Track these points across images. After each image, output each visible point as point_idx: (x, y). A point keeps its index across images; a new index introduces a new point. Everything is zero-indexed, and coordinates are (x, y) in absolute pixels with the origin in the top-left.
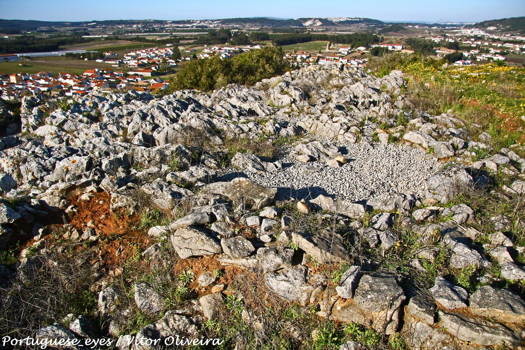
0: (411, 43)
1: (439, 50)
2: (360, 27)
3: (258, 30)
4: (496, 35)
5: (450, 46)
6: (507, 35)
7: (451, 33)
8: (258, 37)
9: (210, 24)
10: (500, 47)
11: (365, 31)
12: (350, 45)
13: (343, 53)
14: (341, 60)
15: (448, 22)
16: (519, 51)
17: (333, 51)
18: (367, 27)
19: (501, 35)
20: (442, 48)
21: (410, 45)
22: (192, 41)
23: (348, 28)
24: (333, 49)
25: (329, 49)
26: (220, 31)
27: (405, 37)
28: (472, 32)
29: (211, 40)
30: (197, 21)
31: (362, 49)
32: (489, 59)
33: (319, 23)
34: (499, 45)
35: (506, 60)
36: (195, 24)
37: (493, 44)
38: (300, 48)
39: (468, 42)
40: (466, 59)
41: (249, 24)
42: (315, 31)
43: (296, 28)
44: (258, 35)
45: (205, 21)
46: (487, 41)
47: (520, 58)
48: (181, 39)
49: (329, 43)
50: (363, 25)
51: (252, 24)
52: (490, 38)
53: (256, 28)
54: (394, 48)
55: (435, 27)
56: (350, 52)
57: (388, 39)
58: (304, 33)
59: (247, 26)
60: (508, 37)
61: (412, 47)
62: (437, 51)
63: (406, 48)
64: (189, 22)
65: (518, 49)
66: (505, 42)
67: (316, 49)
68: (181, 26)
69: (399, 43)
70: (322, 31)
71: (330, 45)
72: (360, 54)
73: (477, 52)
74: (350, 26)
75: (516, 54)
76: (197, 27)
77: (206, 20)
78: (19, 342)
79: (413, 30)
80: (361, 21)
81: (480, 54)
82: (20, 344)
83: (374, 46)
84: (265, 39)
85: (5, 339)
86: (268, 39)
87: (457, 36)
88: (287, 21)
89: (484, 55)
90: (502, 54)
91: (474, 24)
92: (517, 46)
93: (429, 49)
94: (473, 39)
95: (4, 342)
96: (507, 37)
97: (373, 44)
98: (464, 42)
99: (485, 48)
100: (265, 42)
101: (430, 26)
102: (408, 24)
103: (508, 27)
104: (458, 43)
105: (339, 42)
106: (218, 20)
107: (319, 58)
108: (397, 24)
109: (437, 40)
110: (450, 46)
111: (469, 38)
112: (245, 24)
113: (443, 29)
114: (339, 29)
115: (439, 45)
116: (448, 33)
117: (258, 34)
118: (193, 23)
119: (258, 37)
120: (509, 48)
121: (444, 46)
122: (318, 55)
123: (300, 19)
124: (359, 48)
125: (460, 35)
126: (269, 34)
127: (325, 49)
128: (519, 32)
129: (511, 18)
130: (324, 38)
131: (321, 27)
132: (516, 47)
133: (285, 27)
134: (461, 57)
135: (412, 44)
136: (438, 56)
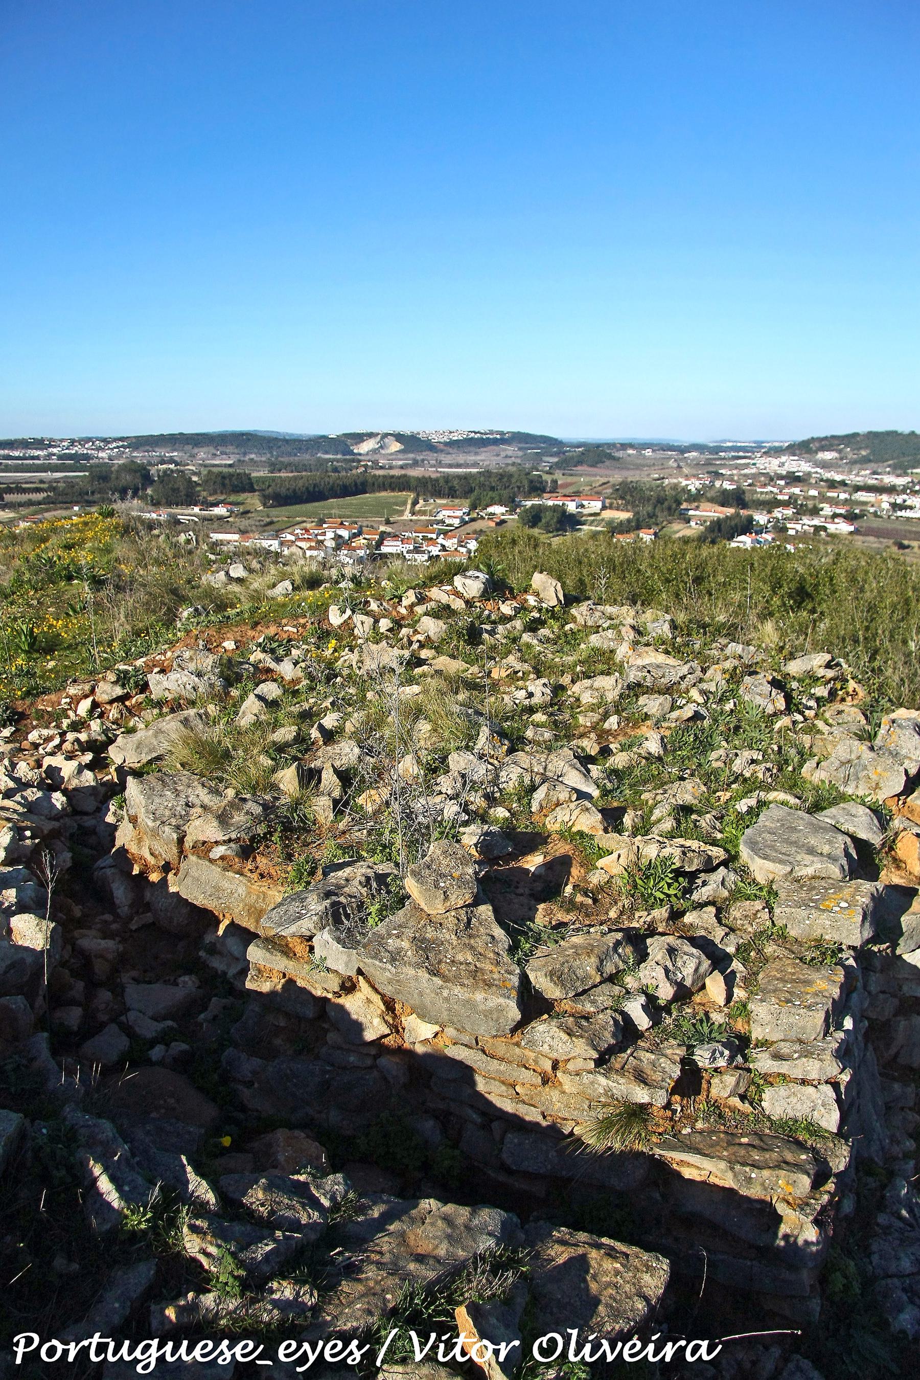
0: (626, 494)
1: (697, 508)
2: (503, 454)
3: (230, 466)
4: (838, 473)
5: (724, 499)
6: (863, 473)
7: (732, 467)
8: (224, 485)
9: (99, 449)
10: (846, 500)
11: (513, 464)
12: (467, 503)
13: (448, 521)
14: (441, 540)
15: (725, 441)
16: (888, 510)
17: (423, 518)
18: (520, 453)
19: (850, 472)
20: (705, 505)
21: (622, 498)
22: (40, 496)
23: (471, 458)
24: (423, 513)
25: (413, 514)
26: (123, 468)
27: (617, 477)
28: (782, 465)
29: (93, 493)
30: (62, 440)
31: (498, 510)
32: (817, 529)
33: (396, 446)
34: (843, 496)
35: (857, 532)
36: (55, 450)
37: (829, 494)
38: (333, 511)
39: (769, 488)
40: (761, 530)
41: (205, 449)
42: (381, 468)
43: (332, 461)
44: (224, 478)
45: (83, 441)
46: (815, 486)
47: (889, 526)
48: (10, 490)
49: (412, 496)
50: (510, 450)
51: (216, 448)
52: (822, 480)
53: (224, 461)
54: (583, 506)
55: (694, 454)
56: (467, 518)
57: (571, 484)
58: (354, 472)
59: (201, 453)
60: (865, 476)
61: (628, 503)
62: (691, 513)
63: (611, 507)
64: (39, 443)
65: (885, 506)
66: (858, 489)
67: (379, 514)
68: (16, 453)
69: (596, 494)
70: (402, 467)
71: (415, 503)
72: (493, 524)
73: (789, 512)
74: (476, 454)
75: (881, 517)
76: (60, 457)
77: (89, 440)
78: (66, 1352)
79: (639, 462)
80: (503, 439)
81: (797, 517)
82: (71, 1358)
83: (529, 504)
84: (243, 490)
85: (23, 1341)
86: (252, 490)
87: (745, 475)
88: (310, 440)
89: (806, 520)
90: (850, 517)
91: (786, 444)
92: (885, 497)
93: (669, 509)
94: (782, 483)
95: (20, 1350)
96: (863, 476)
97: (528, 496)
98: (758, 490)
99: (810, 504)
100: (242, 497)
101: (682, 450)
102: (624, 446)
103: (864, 453)
104: (744, 492)
105: (438, 494)
106: (122, 439)
107: (383, 536)
108: (598, 446)
109: (693, 485)
110: (724, 499)
111: (771, 479)
112: (196, 450)
113: (712, 456)
114: (447, 459)
115: (696, 498)
116: (723, 466)
117: (223, 477)
118: (50, 446)
119: (224, 485)
120: (865, 503)
121: (712, 500)
122: (382, 528)
123: (345, 435)
124: (491, 510)
125: (754, 471)
126: (254, 475)
127: (401, 513)
128: (889, 466)
129: (870, 433)
130: (401, 484)
131: (400, 456)
132: (881, 501)
133: (306, 457)
134: (748, 527)
135: (628, 497)
136: (693, 523)
